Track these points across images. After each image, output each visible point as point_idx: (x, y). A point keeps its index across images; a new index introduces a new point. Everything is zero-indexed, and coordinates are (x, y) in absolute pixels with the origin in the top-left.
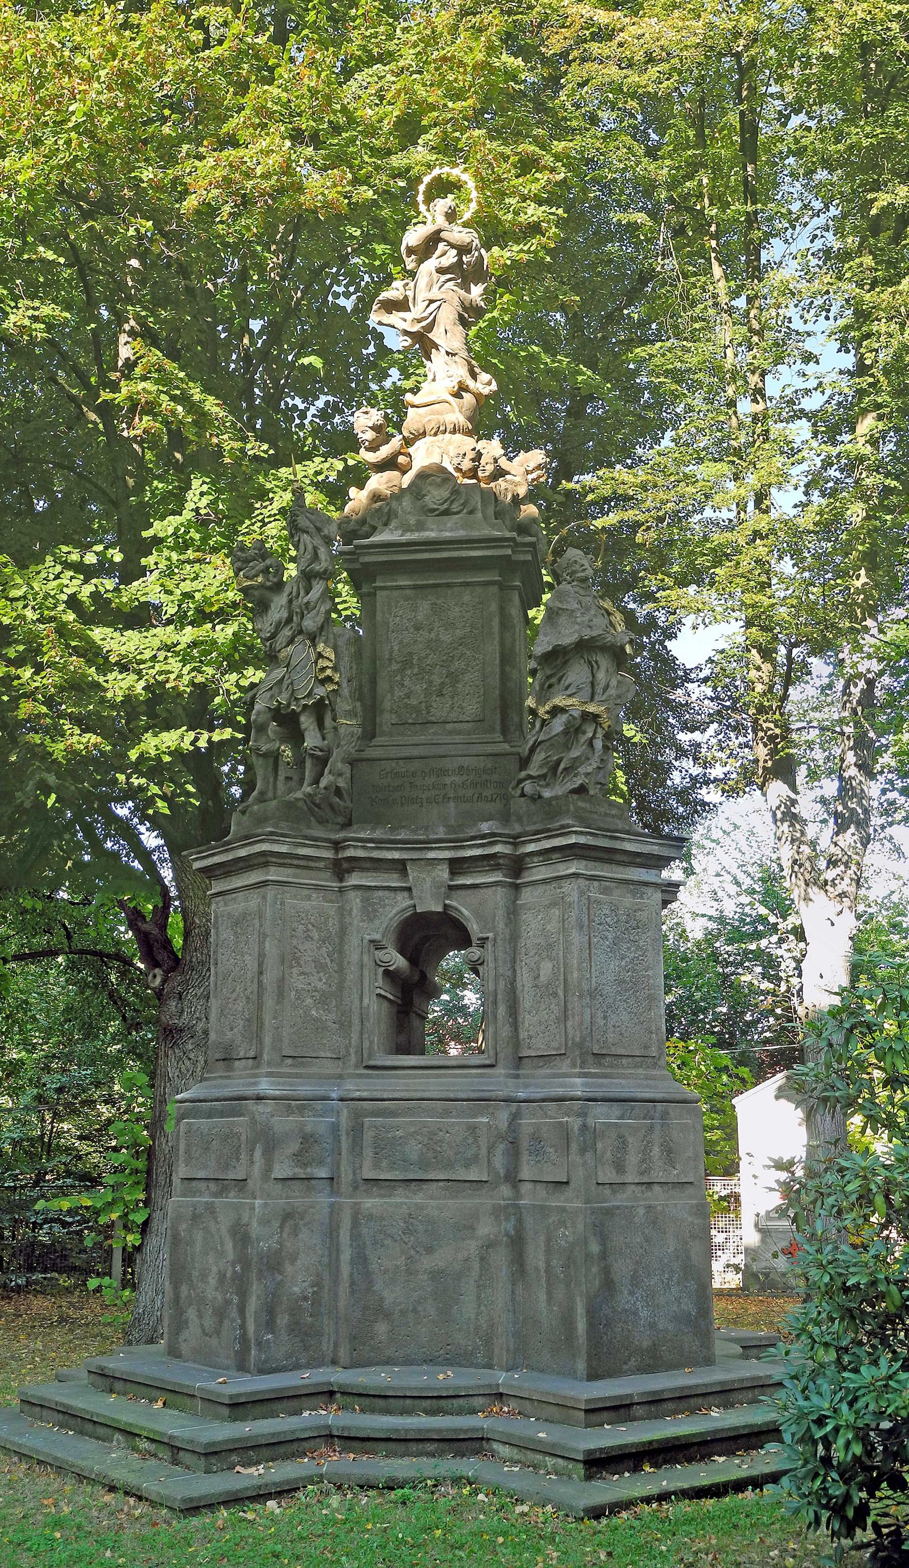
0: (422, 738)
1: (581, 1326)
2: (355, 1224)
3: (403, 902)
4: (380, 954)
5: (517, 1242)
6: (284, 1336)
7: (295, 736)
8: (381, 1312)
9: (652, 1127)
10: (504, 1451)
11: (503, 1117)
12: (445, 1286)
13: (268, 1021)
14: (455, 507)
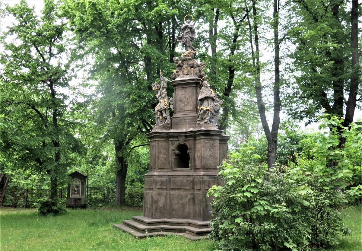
0: (183, 114)
1: (202, 212)
2: (170, 196)
3: (178, 143)
4: (174, 151)
5: (194, 199)
6: (158, 213)
7: (162, 114)
8: (174, 210)
9: (215, 180)
10: (188, 232)
11: (192, 178)
12: (183, 206)
13: (156, 163)
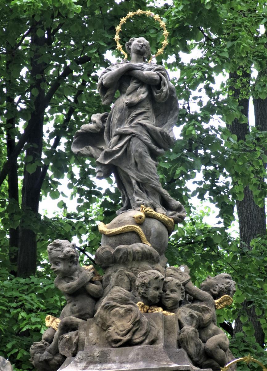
14: (137, 338)
